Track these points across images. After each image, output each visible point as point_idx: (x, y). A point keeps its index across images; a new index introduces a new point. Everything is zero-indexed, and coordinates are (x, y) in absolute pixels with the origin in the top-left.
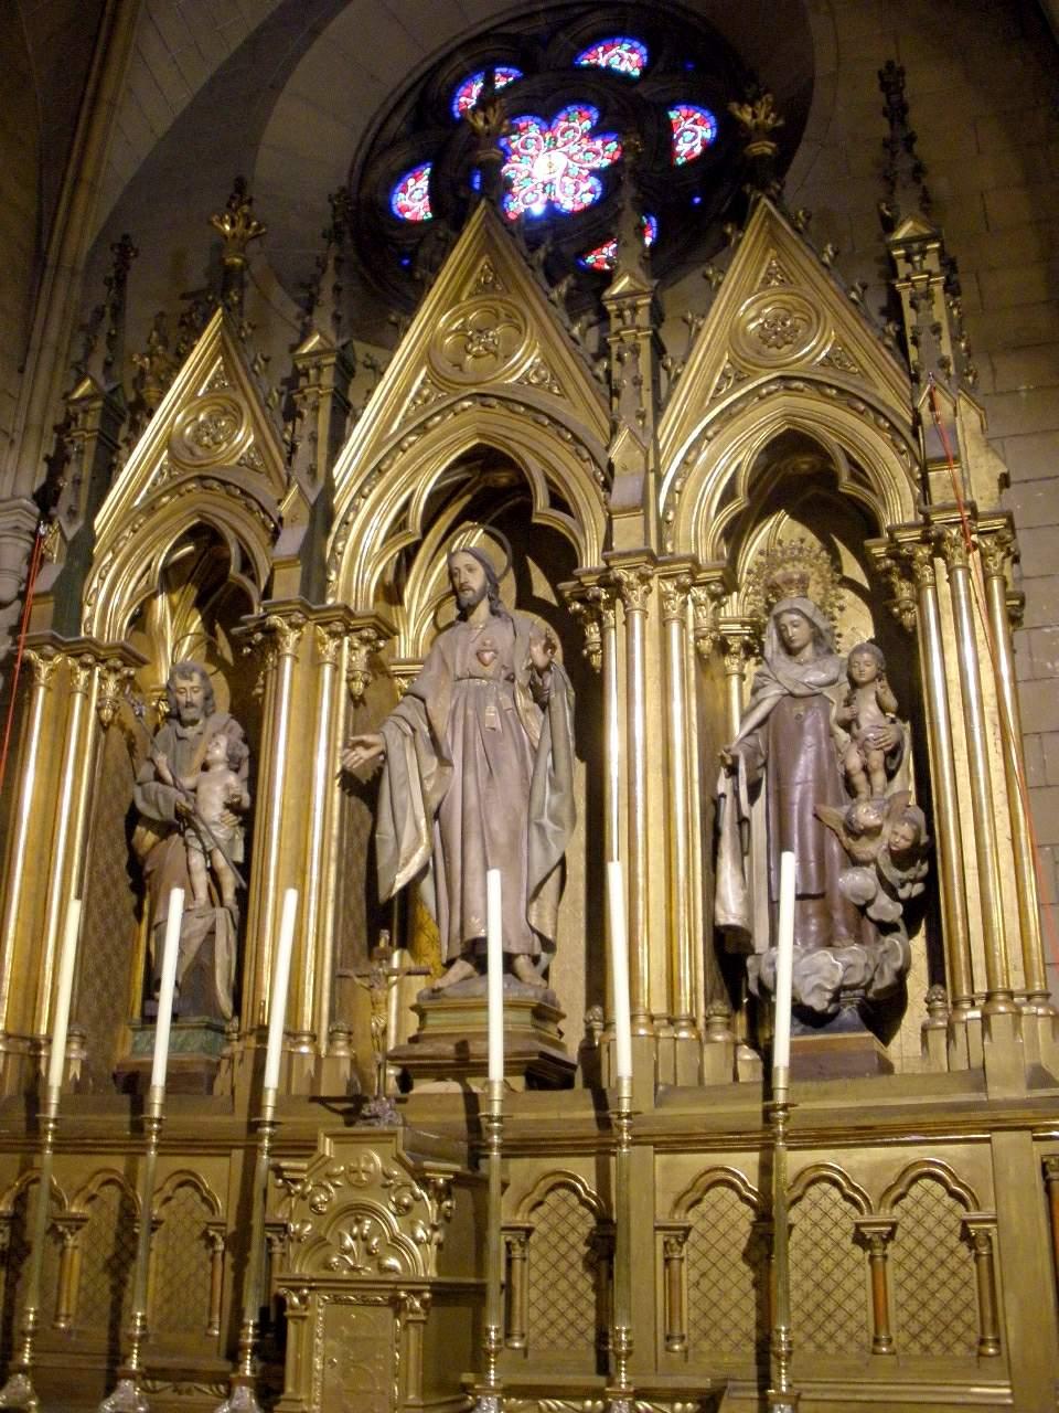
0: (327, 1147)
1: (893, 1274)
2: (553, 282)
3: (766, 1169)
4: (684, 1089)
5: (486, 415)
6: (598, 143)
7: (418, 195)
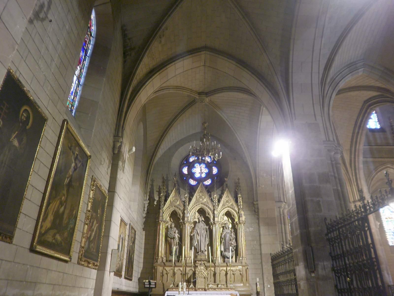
0: (199, 267)
1: (235, 277)
2: (208, 193)
3: (227, 269)
4: (145, 286)
5: (202, 205)
6: (205, 169)
7: (186, 170)
